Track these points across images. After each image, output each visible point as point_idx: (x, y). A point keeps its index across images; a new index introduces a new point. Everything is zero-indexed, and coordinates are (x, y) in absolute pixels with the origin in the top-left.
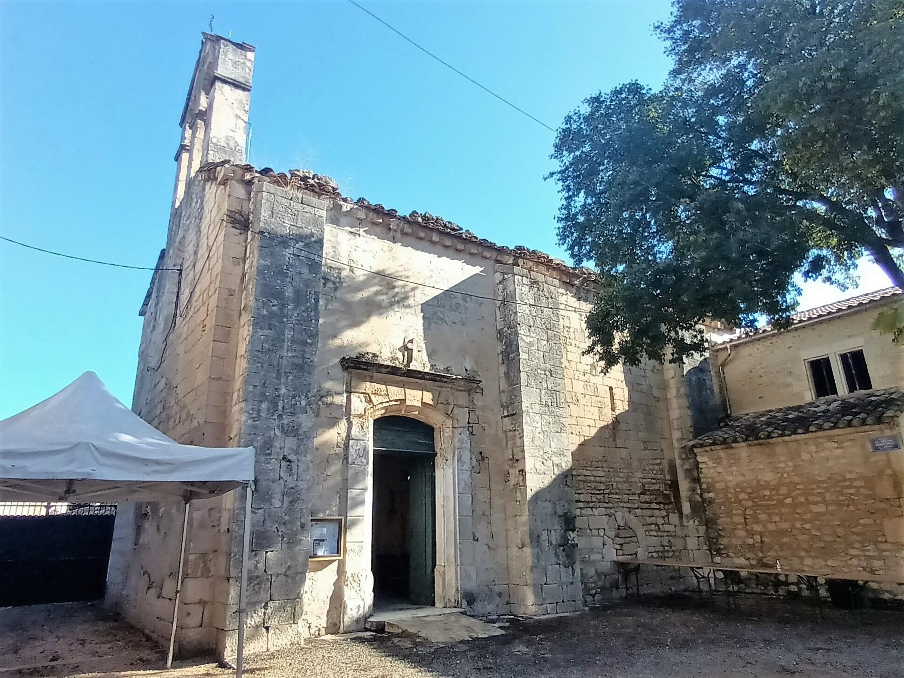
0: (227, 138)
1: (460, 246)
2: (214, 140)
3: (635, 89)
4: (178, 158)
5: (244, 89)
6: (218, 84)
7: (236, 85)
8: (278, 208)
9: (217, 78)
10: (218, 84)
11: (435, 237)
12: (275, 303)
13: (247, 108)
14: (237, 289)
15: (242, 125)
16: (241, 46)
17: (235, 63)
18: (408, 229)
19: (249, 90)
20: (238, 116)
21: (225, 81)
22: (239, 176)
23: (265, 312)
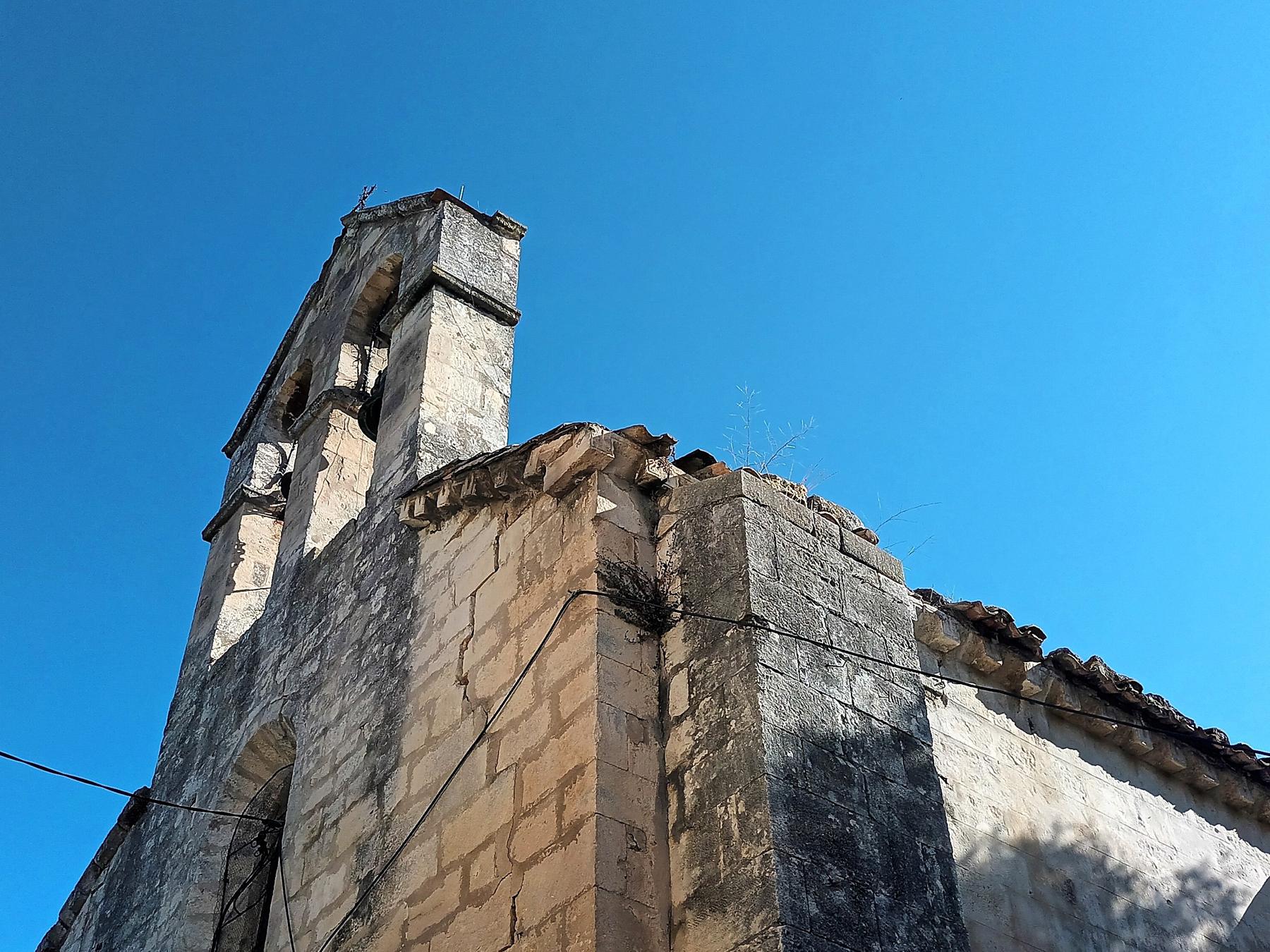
0: (462, 427)
1: (1208, 778)
2: (430, 429)
3: (1009, 620)
4: (221, 527)
5: (501, 318)
6: (438, 296)
7: (483, 305)
8: (789, 555)
9: (435, 280)
10: (438, 296)
11: (1142, 740)
12: (837, 875)
13: (507, 363)
14: (651, 829)
15: (498, 403)
16: (491, 222)
17: (477, 258)
18: (1068, 700)
19: (512, 323)
20: (485, 379)
21: (455, 291)
22: (623, 468)
23: (814, 910)
